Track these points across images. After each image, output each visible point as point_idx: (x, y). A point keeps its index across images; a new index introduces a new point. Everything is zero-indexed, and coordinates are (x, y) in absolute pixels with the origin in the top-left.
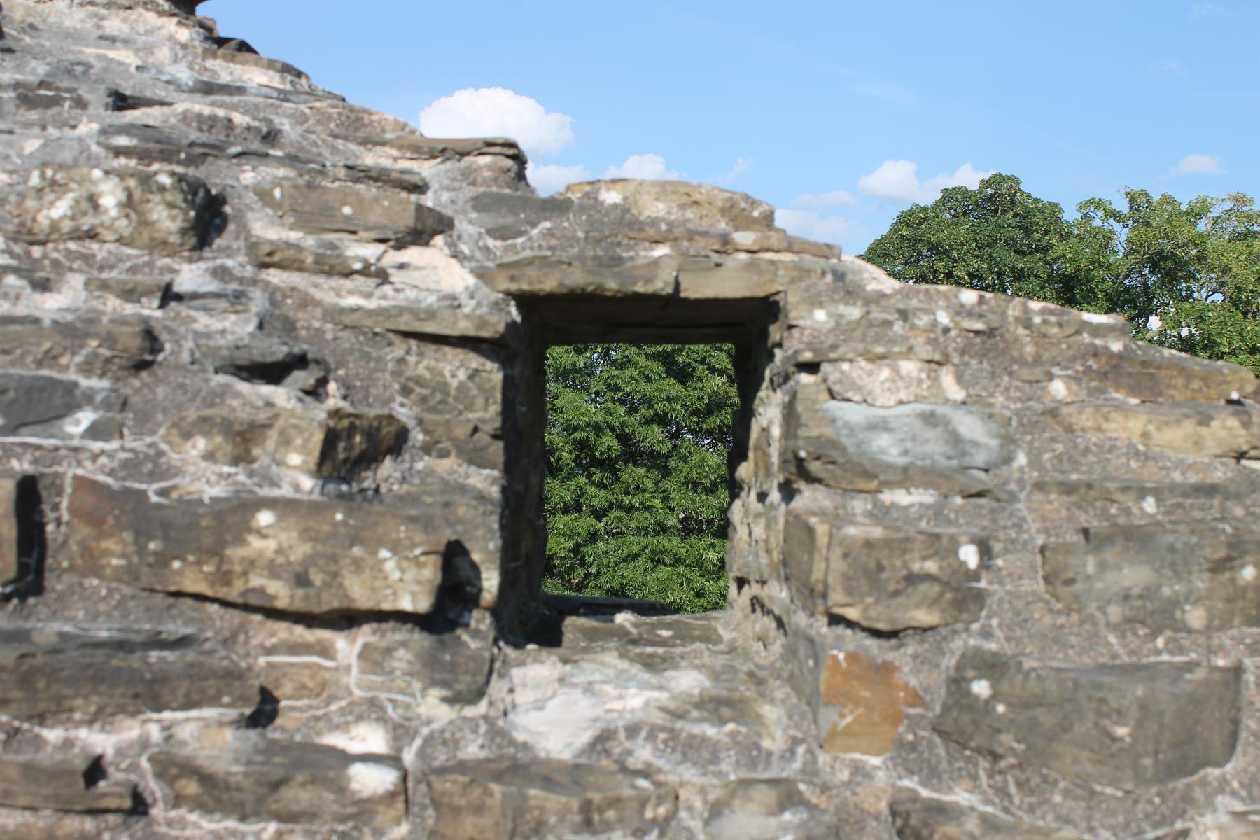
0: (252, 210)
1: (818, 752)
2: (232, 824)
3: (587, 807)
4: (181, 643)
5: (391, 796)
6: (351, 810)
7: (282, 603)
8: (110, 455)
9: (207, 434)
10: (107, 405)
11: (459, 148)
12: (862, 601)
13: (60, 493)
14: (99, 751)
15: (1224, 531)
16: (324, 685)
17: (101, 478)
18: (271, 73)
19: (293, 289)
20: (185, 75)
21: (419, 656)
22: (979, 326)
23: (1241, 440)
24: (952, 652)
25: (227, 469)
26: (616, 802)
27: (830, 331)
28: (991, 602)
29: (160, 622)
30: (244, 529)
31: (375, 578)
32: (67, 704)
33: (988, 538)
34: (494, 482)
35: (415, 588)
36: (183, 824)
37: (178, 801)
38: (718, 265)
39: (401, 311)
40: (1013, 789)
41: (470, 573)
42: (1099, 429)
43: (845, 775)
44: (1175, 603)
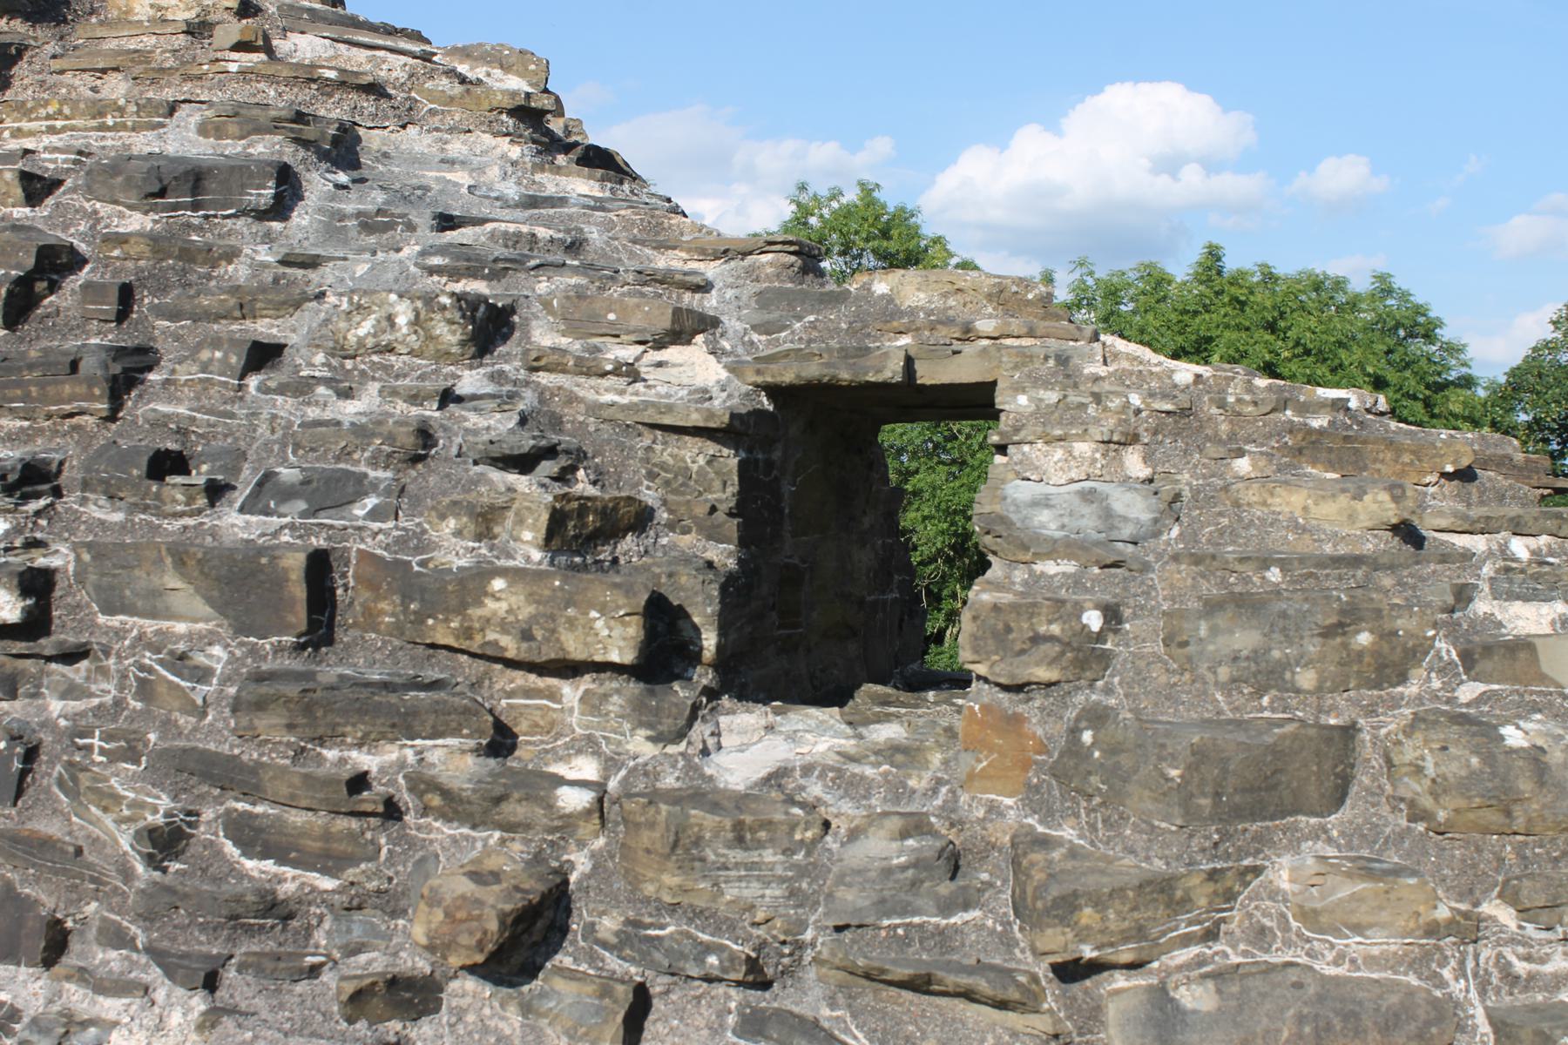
0: (537, 318)
1: (959, 792)
2: (465, 831)
3: (739, 827)
4: (435, 685)
5: (587, 813)
6: (556, 823)
7: (511, 654)
8: (386, 533)
9: (457, 516)
10: (388, 492)
11: (741, 247)
12: (988, 659)
13: (347, 564)
14: (366, 768)
15: (1339, 599)
16: (553, 723)
17: (379, 552)
18: (592, 182)
19: (560, 388)
20: (511, 190)
21: (629, 701)
22: (1169, 407)
23: (1391, 513)
24: (1074, 706)
25: (471, 544)
26: (768, 824)
27: (1031, 414)
28: (1117, 663)
29: (422, 668)
30: (483, 593)
31: (588, 635)
32: (340, 730)
33: (1118, 605)
34: (730, 554)
35: (622, 644)
36: (430, 829)
37: (426, 811)
38: (955, 353)
39: (647, 405)
40: (1100, 825)
41: (692, 634)
42: (1264, 504)
43: (981, 813)
44: (1285, 665)
